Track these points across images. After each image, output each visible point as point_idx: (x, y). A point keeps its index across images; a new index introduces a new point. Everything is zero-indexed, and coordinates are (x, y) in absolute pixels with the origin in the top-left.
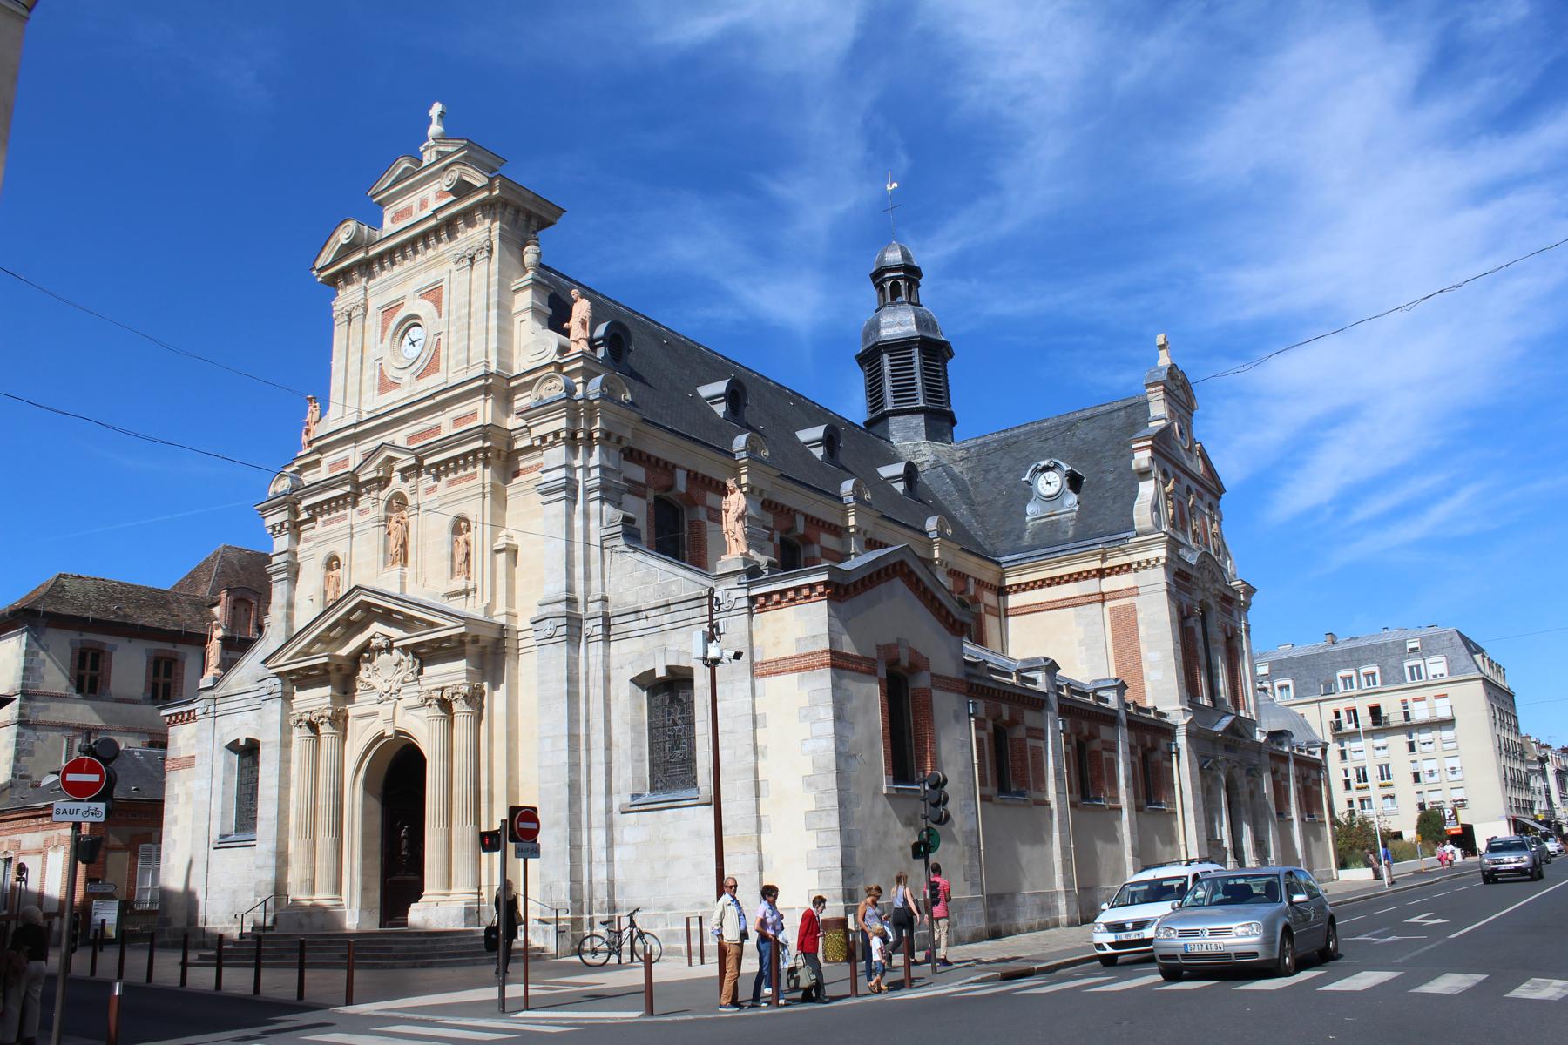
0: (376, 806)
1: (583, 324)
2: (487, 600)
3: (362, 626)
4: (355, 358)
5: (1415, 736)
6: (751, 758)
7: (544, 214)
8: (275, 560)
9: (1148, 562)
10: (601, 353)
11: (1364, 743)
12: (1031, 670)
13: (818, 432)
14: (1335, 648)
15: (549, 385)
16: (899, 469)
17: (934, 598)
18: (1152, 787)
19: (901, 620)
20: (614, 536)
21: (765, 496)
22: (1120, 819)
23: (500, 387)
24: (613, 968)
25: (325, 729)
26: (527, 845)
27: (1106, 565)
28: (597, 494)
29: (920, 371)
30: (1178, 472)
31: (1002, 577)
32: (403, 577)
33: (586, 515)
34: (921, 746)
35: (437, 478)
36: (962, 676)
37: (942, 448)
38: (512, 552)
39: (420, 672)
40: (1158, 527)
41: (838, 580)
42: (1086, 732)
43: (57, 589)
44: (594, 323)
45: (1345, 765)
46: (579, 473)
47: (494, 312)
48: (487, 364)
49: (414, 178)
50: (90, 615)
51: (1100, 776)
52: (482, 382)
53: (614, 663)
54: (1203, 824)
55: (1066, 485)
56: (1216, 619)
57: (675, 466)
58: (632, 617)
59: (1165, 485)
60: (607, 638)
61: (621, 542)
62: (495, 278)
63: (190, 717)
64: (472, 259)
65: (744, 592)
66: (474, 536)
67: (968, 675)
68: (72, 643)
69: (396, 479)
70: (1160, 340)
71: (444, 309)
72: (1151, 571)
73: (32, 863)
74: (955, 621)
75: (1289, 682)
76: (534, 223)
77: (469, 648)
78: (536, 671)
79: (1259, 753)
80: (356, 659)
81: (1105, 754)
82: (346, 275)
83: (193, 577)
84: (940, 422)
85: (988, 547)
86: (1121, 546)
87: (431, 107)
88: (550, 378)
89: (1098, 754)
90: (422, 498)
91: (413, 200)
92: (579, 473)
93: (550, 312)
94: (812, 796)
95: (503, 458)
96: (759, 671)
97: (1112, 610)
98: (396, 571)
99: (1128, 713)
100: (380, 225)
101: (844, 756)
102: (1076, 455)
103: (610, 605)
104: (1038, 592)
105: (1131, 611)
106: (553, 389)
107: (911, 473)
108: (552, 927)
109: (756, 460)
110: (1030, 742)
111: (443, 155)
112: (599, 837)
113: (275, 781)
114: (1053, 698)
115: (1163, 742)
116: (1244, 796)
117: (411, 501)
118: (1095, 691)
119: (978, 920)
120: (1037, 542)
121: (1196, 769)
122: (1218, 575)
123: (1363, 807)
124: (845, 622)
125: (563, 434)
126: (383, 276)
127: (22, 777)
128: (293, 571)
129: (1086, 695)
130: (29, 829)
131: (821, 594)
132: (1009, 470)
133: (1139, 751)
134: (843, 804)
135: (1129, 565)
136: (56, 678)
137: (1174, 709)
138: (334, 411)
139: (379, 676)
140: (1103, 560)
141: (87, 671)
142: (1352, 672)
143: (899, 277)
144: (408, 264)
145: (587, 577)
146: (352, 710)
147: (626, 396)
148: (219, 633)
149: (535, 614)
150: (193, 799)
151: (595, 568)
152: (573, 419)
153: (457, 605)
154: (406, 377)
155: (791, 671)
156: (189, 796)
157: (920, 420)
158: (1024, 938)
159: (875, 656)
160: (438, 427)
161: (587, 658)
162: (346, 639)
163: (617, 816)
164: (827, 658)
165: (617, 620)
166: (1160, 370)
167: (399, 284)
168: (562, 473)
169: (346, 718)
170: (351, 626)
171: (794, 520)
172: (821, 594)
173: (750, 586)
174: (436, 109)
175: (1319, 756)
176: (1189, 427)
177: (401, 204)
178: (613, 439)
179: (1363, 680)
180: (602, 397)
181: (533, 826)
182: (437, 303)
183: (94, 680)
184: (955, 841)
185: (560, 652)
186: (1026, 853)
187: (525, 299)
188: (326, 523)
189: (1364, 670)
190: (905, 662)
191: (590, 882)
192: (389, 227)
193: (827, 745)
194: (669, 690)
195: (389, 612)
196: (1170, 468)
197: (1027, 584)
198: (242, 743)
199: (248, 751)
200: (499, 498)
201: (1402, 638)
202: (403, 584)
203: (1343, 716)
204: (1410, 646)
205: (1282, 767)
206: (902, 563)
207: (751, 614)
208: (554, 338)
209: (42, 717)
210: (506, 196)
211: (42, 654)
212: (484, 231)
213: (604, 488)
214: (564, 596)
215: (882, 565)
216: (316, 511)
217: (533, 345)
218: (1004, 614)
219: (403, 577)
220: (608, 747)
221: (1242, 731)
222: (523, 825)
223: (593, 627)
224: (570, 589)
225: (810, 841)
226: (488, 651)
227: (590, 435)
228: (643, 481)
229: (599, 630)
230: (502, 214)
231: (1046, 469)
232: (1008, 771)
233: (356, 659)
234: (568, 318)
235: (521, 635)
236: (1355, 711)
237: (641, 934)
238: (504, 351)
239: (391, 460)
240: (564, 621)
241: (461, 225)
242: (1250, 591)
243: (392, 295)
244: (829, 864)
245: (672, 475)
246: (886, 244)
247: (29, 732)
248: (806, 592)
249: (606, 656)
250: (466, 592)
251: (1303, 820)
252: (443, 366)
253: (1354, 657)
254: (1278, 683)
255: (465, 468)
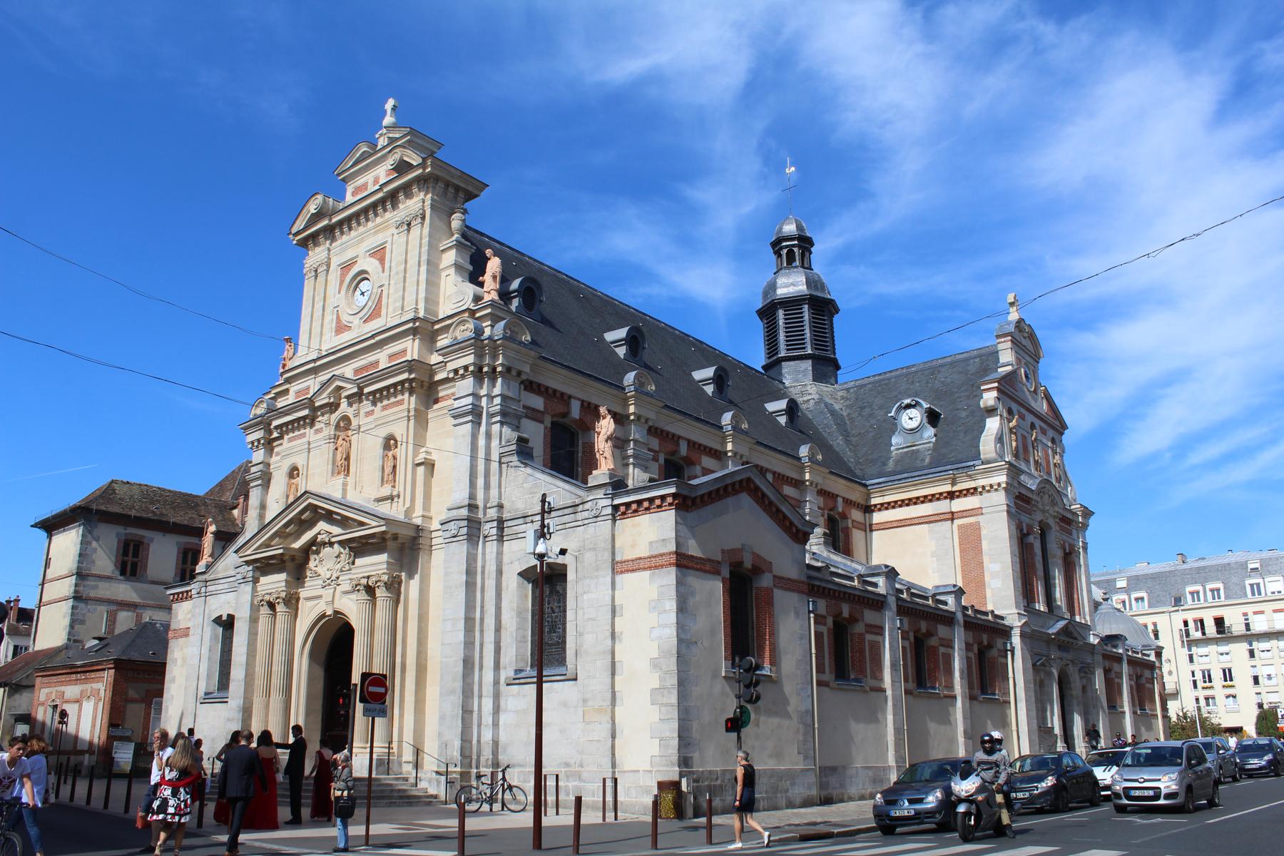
0: (320, 673)
1: (494, 277)
2: (408, 505)
3: (311, 524)
4: (319, 306)
5: (1255, 645)
6: (609, 642)
7: (470, 188)
8: (253, 470)
9: (991, 486)
10: (515, 303)
11: (1213, 649)
12: (873, 575)
13: (709, 372)
14: (1185, 566)
15: (462, 328)
16: (782, 404)
17: (778, 510)
18: (986, 677)
19: (745, 528)
20: (509, 454)
21: (650, 424)
22: (954, 705)
23: (425, 329)
24: (484, 814)
25: (280, 608)
26: (377, 706)
27: (956, 488)
28: (498, 418)
29: (808, 324)
30: (1023, 411)
31: (868, 498)
32: (345, 485)
33: (489, 436)
34: (761, 637)
35: (374, 404)
36: (803, 579)
37: (826, 388)
38: (430, 466)
39: (353, 563)
40: (1002, 457)
41: (685, 492)
42: (924, 630)
43: (108, 492)
44: (504, 280)
45: (1193, 667)
46: (484, 400)
47: (424, 268)
48: (416, 310)
49: (371, 157)
50: (133, 513)
51: (937, 667)
52: (411, 325)
53: (506, 559)
54: (1034, 713)
55: (925, 420)
56: (1054, 538)
57: (570, 397)
58: (521, 521)
59: (1009, 421)
60: (500, 538)
61: (515, 458)
62: (426, 240)
63: (186, 596)
64: (409, 225)
65: (608, 502)
66: (400, 452)
67: (809, 577)
68: (118, 534)
69: (344, 403)
70: (1011, 298)
71: (387, 265)
72: (993, 494)
73: (71, 709)
74: (798, 531)
75: (1144, 595)
76: (461, 195)
77: (390, 544)
78: (444, 564)
79: (1093, 653)
80: (307, 550)
81: (942, 650)
82: (314, 238)
83: (221, 486)
84: (826, 366)
85: (858, 472)
86: (968, 471)
87: (386, 102)
88: (463, 322)
89: (935, 649)
90: (363, 420)
91: (368, 178)
92: (484, 400)
93: (471, 268)
94: (656, 675)
95: (426, 387)
96: (618, 567)
97: (960, 527)
98: (340, 479)
99: (965, 615)
100: (344, 198)
101: (685, 643)
102: (937, 395)
103: (505, 510)
104: (898, 510)
105: (976, 528)
106: (465, 331)
107: (792, 409)
108: (443, 778)
109: (643, 393)
110: (869, 637)
111: (392, 140)
112: (488, 704)
113: (244, 650)
114: (892, 600)
115: (999, 642)
116: (1076, 690)
117: (354, 422)
118: (934, 595)
119: (809, 788)
120: (899, 468)
121: (1030, 665)
122: (1058, 499)
123: (1208, 705)
124: (691, 529)
125: (471, 368)
126: (343, 239)
127: (75, 641)
128: (266, 479)
129: (926, 598)
130: (70, 683)
131: (670, 504)
132: (881, 408)
133: (975, 648)
134: (682, 684)
135: (975, 489)
136: (104, 562)
137: (1012, 615)
138: (302, 350)
139: (324, 565)
140: (953, 484)
141: (130, 558)
142: (1198, 588)
143: (794, 246)
144: (361, 229)
145: (487, 486)
146: (303, 593)
147: (527, 337)
148: (213, 528)
149: (444, 517)
150: (187, 665)
151: (494, 480)
152: (479, 355)
153: (385, 509)
154: (356, 321)
155: (645, 569)
156: (184, 660)
157: (808, 365)
158: (852, 806)
159: (720, 559)
160: (377, 362)
161: (484, 554)
162: (298, 535)
163: (503, 687)
164: (673, 559)
165: (510, 523)
166: (1009, 323)
167: (354, 246)
168: (470, 400)
169: (298, 600)
170: (302, 524)
171: (678, 445)
172: (670, 504)
173: (613, 497)
174: (390, 103)
175: (1152, 658)
176: (1035, 373)
177: (360, 181)
178: (514, 373)
179: (1209, 594)
180: (504, 338)
181: (382, 690)
182: (382, 261)
183: (134, 566)
184: (787, 716)
185: (461, 549)
186: (859, 730)
187: (450, 257)
188: (290, 440)
189: (1209, 586)
190: (748, 564)
191: (479, 741)
192: (349, 199)
193: (671, 633)
194: (548, 582)
195: (330, 513)
196: (1015, 407)
197: (889, 503)
198: (224, 618)
199: (227, 624)
200: (421, 420)
201: (1243, 560)
202: (344, 491)
203: (1191, 625)
204: (1251, 566)
205: (1116, 667)
206: (749, 480)
207: (614, 520)
208: (471, 289)
209: (92, 594)
210: (437, 172)
211: (94, 544)
212: (419, 202)
213: (503, 413)
214: (466, 502)
215: (729, 481)
216: (284, 429)
217: (455, 293)
218: (869, 528)
219: (345, 485)
220: (498, 629)
221: (1075, 634)
222: (372, 689)
223: (490, 529)
224: (472, 496)
225: (654, 714)
226: (405, 546)
227: (494, 369)
228: (541, 408)
229: (494, 531)
230: (434, 188)
231: (909, 406)
232: (845, 659)
233: (307, 550)
234: (483, 273)
235: (434, 535)
236: (1202, 621)
237: (510, 787)
238: (431, 300)
239: (340, 388)
240: (465, 523)
241: (401, 197)
242: (1088, 513)
243: (349, 254)
244: (668, 734)
245: (568, 405)
246: (785, 220)
247: (82, 605)
248: (658, 502)
249: (500, 554)
250: (391, 498)
251: (1135, 713)
252: (383, 312)
253: (1202, 575)
254: (1134, 595)
255: (395, 395)
